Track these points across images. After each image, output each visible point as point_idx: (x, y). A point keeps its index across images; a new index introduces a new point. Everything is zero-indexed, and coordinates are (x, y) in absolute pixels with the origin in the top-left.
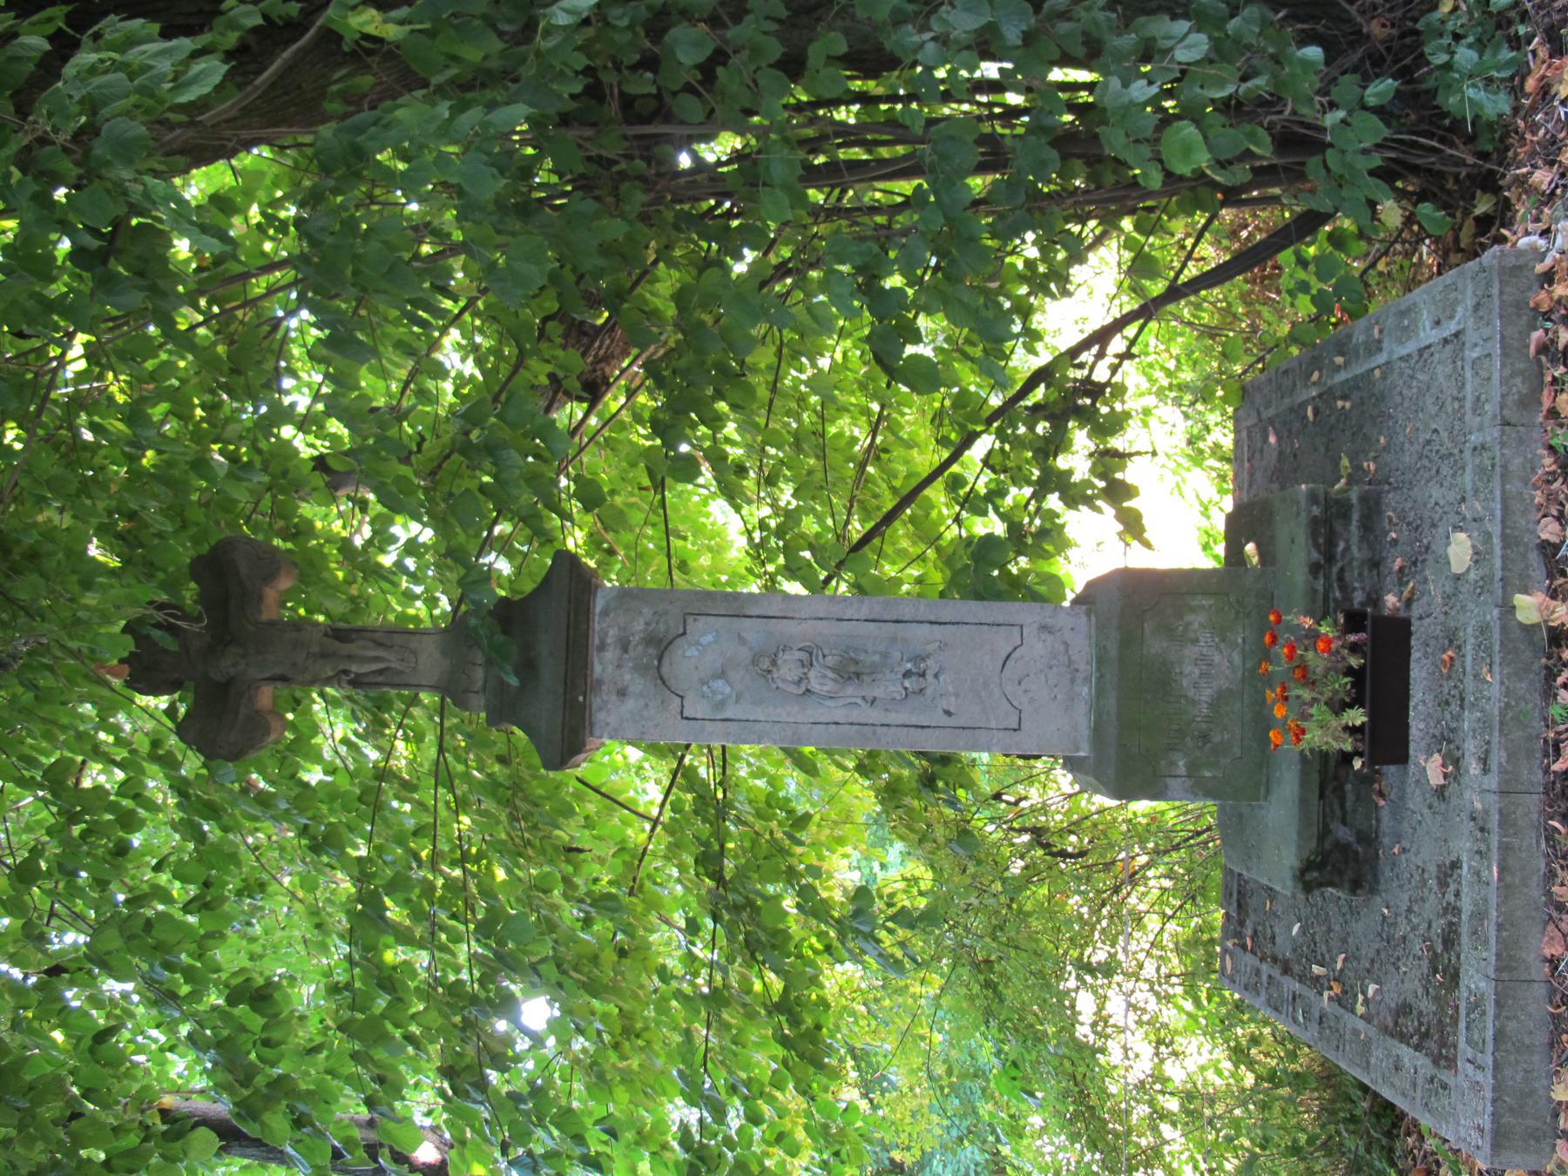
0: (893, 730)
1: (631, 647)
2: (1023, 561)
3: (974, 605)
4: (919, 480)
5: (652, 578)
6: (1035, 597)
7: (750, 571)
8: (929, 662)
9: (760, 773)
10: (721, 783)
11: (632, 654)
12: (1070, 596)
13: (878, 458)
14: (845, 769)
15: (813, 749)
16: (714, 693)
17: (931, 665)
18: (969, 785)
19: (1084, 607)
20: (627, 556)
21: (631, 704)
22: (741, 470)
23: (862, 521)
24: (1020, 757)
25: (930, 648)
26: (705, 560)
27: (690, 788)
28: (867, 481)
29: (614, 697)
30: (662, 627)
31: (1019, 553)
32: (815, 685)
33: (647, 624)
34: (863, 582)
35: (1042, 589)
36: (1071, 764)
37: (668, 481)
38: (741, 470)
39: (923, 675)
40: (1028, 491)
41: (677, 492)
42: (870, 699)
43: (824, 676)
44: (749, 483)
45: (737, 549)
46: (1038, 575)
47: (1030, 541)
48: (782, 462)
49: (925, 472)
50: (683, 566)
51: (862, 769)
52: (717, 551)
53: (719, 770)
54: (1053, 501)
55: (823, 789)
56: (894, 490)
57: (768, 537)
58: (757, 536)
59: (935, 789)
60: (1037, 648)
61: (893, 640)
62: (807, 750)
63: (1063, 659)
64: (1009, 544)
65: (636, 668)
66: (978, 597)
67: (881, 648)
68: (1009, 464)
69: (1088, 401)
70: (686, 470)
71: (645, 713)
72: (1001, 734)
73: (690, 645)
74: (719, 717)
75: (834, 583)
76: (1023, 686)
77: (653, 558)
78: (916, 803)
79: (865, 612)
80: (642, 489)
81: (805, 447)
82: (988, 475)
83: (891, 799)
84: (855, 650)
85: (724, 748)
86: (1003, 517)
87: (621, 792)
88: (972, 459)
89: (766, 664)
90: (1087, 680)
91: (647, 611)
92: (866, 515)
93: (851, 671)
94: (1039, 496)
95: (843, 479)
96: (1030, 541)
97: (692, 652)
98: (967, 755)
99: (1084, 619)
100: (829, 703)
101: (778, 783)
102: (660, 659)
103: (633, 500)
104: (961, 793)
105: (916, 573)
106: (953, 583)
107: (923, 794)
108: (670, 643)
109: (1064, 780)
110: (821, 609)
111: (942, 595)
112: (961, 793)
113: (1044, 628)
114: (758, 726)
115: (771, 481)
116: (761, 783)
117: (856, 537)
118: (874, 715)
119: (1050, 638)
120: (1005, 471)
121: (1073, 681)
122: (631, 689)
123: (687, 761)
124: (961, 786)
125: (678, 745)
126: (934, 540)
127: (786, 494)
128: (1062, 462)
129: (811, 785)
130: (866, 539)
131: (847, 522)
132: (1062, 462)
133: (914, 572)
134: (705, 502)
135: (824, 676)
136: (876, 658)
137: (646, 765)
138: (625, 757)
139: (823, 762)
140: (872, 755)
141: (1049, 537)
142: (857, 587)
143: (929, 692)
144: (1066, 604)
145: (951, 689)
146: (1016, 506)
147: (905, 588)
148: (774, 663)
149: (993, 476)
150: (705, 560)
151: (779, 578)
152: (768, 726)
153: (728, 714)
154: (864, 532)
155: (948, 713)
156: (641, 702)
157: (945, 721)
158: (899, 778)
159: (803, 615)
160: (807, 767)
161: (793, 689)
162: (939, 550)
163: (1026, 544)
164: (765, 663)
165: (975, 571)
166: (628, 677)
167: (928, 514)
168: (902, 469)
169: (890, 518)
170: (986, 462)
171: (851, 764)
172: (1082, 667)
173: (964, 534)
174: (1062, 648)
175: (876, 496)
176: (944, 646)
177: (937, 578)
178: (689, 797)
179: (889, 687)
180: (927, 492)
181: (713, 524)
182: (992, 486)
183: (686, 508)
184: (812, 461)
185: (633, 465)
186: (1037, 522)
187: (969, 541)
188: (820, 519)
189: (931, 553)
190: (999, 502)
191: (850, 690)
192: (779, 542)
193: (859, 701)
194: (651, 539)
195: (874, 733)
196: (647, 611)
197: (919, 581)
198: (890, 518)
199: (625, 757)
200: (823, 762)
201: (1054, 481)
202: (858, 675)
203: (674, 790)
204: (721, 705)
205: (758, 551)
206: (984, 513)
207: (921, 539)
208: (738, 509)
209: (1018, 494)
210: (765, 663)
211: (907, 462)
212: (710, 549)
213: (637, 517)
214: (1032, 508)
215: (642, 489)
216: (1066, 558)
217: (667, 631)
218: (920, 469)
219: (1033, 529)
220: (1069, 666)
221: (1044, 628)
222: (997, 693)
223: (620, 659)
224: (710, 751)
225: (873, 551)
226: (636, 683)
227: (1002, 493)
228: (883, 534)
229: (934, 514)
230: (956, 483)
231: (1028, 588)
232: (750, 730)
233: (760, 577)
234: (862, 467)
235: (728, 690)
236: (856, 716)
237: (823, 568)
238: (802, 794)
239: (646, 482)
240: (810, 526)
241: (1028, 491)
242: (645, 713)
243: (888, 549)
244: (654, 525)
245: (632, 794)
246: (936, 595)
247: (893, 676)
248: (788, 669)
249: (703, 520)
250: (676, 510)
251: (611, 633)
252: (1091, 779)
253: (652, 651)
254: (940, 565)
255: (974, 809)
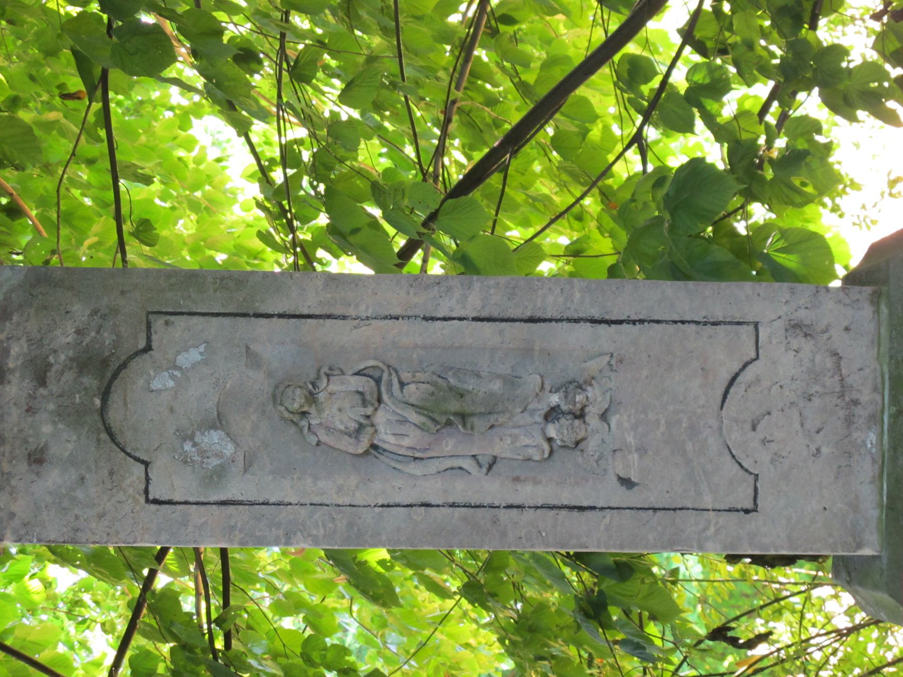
0: (529, 514)
1: (51, 375)
2: (759, 212)
3: (669, 288)
4: (568, 69)
5: (92, 248)
6: (779, 274)
7: (265, 237)
8: (590, 392)
9: (289, 605)
10: (219, 622)
11: (53, 387)
12: (841, 272)
13: (494, 33)
14: (442, 592)
15: (383, 553)
16: (203, 453)
17: (595, 397)
18: (666, 613)
19: (868, 290)
20: (43, 218)
21: (54, 478)
22: (247, 57)
23: (468, 150)
24: (758, 560)
25: (593, 366)
26: (186, 226)
27: (165, 632)
28: (474, 75)
29: (23, 467)
30: (108, 338)
31: (751, 196)
32: (387, 438)
33: (78, 332)
34: (472, 250)
35: (789, 261)
36: (849, 572)
37: (115, 75)
38: (247, 57)
39: (580, 415)
40: (763, 89)
41: (131, 96)
42: (485, 461)
43: (404, 421)
44: (262, 82)
45: (243, 208)
46: (784, 234)
47: (769, 174)
48: (321, 44)
49: (578, 54)
50: (145, 230)
51: (474, 591)
52: (205, 209)
53: (216, 601)
54: (810, 104)
55: (405, 631)
56: (523, 88)
57: (298, 177)
58: (278, 176)
59: (606, 625)
60: (784, 364)
61: (527, 352)
62: (375, 556)
63: (832, 382)
64: (731, 180)
65: (61, 414)
66: (677, 273)
67: (504, 369)
68: (732, 39)
69: (876, 84)
70: (150, 56)
71: (80, 494)
72: (724, 518)
73: (159, 369)
74: (214, 498)
75: (417, 258)
76: (760, 434)
77: (88, 220)
78: (572, 651)
79: (474, 304)
80: (66, 96)
81: (363, 14)
82: (691, 56)
83: (527, 644)
84: (457, 372)
85: (224, 553)
86: (720, 132)
87: (41, 647)
88: (664, 35)
89: (297, 401)
90: (875, 419)
91: (80, 311)
92: (475, 132)
93: (452, 410)
94: (783, 94)
95: (430, 71)
96: (769, 174)
97: (163, 381)
98: (662, 562)
99: (867, 311)
100: (415, 469)
101: (324, 622)
102: (105, 395)
103: (52, 116)
104: (652, 629)
105: (564, 241)
106: (631, 253)
107: (584, 634)
108: (124, 366)
109: (837, 605)
110: (395, 298)
111: (613, 272)
112: (652, 629)
113: (796, 327)
114: (284, 514)
115: (300, 72)
116: (290, 623)
117: (456, 176)
118: (494, 489)
119: (807, 346)
120: (723, 52)
121: (849, 421)
122: (54, 450)
123: (161, 581)
124: (653, 618)
125: (142, 552)
126: (596, 179)
127: (328, 98)
128: (826, 32)
129: (384, 625)
130: (475, 178)
131: (440, 151)
132: (826, 32)
133: (560, 238)
134: (185, 117)
135: (404, 421)
136: (496, 386)
137: (86, 598)
138: (47, 585)
139: (404, 580)
140: (492, 565)
141: (801, 169)
142: (463, 262)
143: (592, 445)
144: (836, 284)
145: (630, 439)
146: (741, 115)
147: (546, 267)
148: (312, 398)
149: (698, 58)
150: (186, 226)
151: (321, 253)
152: (303, 512)
153: (233, 491)
154: (469, 165)
155: (626, 482)
156: (73, 475)
157: (620, 496)
158: (542, 607)
159: (362, 312)
160: (374, 588)
161: (346, 444)
162: (606, 196)
163: (762, 179)
164: (295, 400)
165: (672, 228)
166: (47, 429)
167: (585, 133)
168: (538, 54)
169: (517, 138)
170: (688, 35)
171: (454, 585)
172: (866, 396)
173: (650, 168)
174: (829, 363)
175: (491, 101)
176: (617, 362)
177: (604, 246)
178: (166, 648)
179: (521, 438)
180: (582, 91)
181: (198, 161)
182: (699, 78)
183: (149, 130)
184: (377, 41)
185: (51, 53)
186: (781, 143)
187: (660, 177)
188: (392, 145)
189: (591, 203)
190: (711, 105)
191: (449, 444)
192: (317, 187)
193: (467, 464)
194: (86, 187)
195: (495, 521)
196: (80, 311)
197: (575, 252)
198: (517, 138)
199: (47, 585)
200: (404, 580)
201: (810, 67)
202: (463, 417)
203: (138, 640)
204: (218, 475)
205: (281, 203)
206: (687, 127)
207: (575, 177)
208: (243, 129)
209: (745, 96)
210: (295, 400)
211: (547, 42)
212: (194, 206)
213: (59, 148)
214: (771, 119)
215: (66, 96)
216: (835, 209)
217: (116, 344)
218: (571, 52)
219: (775, 154)
220: (842, 396)
221: (796, 327)
222: (714, 445)
223: (32, 397)
224: (200, 566)
225: (487, 196)
226: (63, 441)
227: (718, 87)
228: (505, 169)
229: (595, 133)
230: (635, 73)
231: (767, 258)
232: (271, 521)
233: (284, 249)
234: (466, 48)
235: (229, 449)
236: (460, 490)
237: (400, 229)
238: (369, 643)
239: (76, 84)
240: (372, 156)
241: (763, 89)
242: (80, 494)
243: (515, 194)
244: (90, 162)
245: (61, 649)
246: (604, 275)
247: (527, 418)
248: (338, 410)
249: (181, 153)
250: (131, 134)
251: (15, 350)
252: (884, 597)
253: (90, 381)
254: (609, 223)
255: (676, 659)
